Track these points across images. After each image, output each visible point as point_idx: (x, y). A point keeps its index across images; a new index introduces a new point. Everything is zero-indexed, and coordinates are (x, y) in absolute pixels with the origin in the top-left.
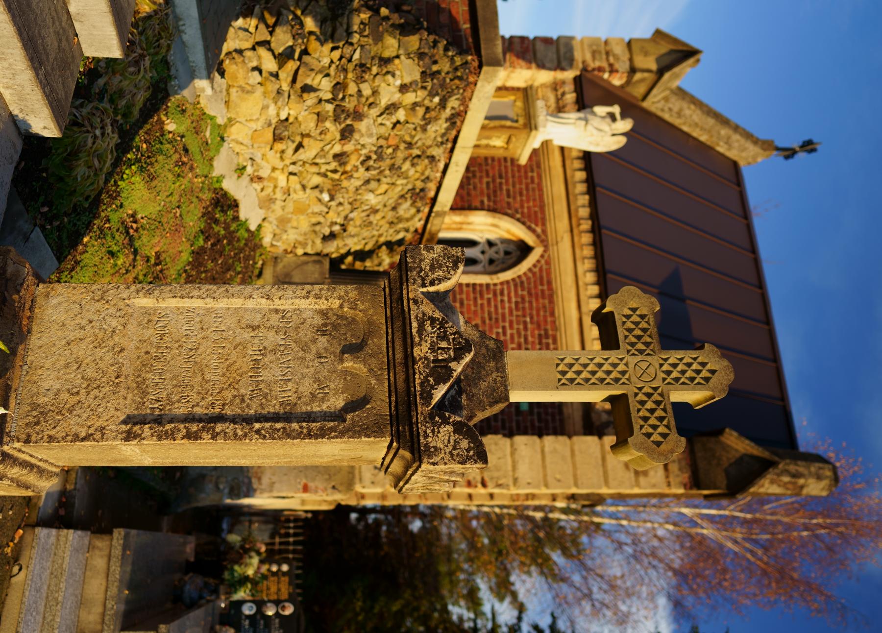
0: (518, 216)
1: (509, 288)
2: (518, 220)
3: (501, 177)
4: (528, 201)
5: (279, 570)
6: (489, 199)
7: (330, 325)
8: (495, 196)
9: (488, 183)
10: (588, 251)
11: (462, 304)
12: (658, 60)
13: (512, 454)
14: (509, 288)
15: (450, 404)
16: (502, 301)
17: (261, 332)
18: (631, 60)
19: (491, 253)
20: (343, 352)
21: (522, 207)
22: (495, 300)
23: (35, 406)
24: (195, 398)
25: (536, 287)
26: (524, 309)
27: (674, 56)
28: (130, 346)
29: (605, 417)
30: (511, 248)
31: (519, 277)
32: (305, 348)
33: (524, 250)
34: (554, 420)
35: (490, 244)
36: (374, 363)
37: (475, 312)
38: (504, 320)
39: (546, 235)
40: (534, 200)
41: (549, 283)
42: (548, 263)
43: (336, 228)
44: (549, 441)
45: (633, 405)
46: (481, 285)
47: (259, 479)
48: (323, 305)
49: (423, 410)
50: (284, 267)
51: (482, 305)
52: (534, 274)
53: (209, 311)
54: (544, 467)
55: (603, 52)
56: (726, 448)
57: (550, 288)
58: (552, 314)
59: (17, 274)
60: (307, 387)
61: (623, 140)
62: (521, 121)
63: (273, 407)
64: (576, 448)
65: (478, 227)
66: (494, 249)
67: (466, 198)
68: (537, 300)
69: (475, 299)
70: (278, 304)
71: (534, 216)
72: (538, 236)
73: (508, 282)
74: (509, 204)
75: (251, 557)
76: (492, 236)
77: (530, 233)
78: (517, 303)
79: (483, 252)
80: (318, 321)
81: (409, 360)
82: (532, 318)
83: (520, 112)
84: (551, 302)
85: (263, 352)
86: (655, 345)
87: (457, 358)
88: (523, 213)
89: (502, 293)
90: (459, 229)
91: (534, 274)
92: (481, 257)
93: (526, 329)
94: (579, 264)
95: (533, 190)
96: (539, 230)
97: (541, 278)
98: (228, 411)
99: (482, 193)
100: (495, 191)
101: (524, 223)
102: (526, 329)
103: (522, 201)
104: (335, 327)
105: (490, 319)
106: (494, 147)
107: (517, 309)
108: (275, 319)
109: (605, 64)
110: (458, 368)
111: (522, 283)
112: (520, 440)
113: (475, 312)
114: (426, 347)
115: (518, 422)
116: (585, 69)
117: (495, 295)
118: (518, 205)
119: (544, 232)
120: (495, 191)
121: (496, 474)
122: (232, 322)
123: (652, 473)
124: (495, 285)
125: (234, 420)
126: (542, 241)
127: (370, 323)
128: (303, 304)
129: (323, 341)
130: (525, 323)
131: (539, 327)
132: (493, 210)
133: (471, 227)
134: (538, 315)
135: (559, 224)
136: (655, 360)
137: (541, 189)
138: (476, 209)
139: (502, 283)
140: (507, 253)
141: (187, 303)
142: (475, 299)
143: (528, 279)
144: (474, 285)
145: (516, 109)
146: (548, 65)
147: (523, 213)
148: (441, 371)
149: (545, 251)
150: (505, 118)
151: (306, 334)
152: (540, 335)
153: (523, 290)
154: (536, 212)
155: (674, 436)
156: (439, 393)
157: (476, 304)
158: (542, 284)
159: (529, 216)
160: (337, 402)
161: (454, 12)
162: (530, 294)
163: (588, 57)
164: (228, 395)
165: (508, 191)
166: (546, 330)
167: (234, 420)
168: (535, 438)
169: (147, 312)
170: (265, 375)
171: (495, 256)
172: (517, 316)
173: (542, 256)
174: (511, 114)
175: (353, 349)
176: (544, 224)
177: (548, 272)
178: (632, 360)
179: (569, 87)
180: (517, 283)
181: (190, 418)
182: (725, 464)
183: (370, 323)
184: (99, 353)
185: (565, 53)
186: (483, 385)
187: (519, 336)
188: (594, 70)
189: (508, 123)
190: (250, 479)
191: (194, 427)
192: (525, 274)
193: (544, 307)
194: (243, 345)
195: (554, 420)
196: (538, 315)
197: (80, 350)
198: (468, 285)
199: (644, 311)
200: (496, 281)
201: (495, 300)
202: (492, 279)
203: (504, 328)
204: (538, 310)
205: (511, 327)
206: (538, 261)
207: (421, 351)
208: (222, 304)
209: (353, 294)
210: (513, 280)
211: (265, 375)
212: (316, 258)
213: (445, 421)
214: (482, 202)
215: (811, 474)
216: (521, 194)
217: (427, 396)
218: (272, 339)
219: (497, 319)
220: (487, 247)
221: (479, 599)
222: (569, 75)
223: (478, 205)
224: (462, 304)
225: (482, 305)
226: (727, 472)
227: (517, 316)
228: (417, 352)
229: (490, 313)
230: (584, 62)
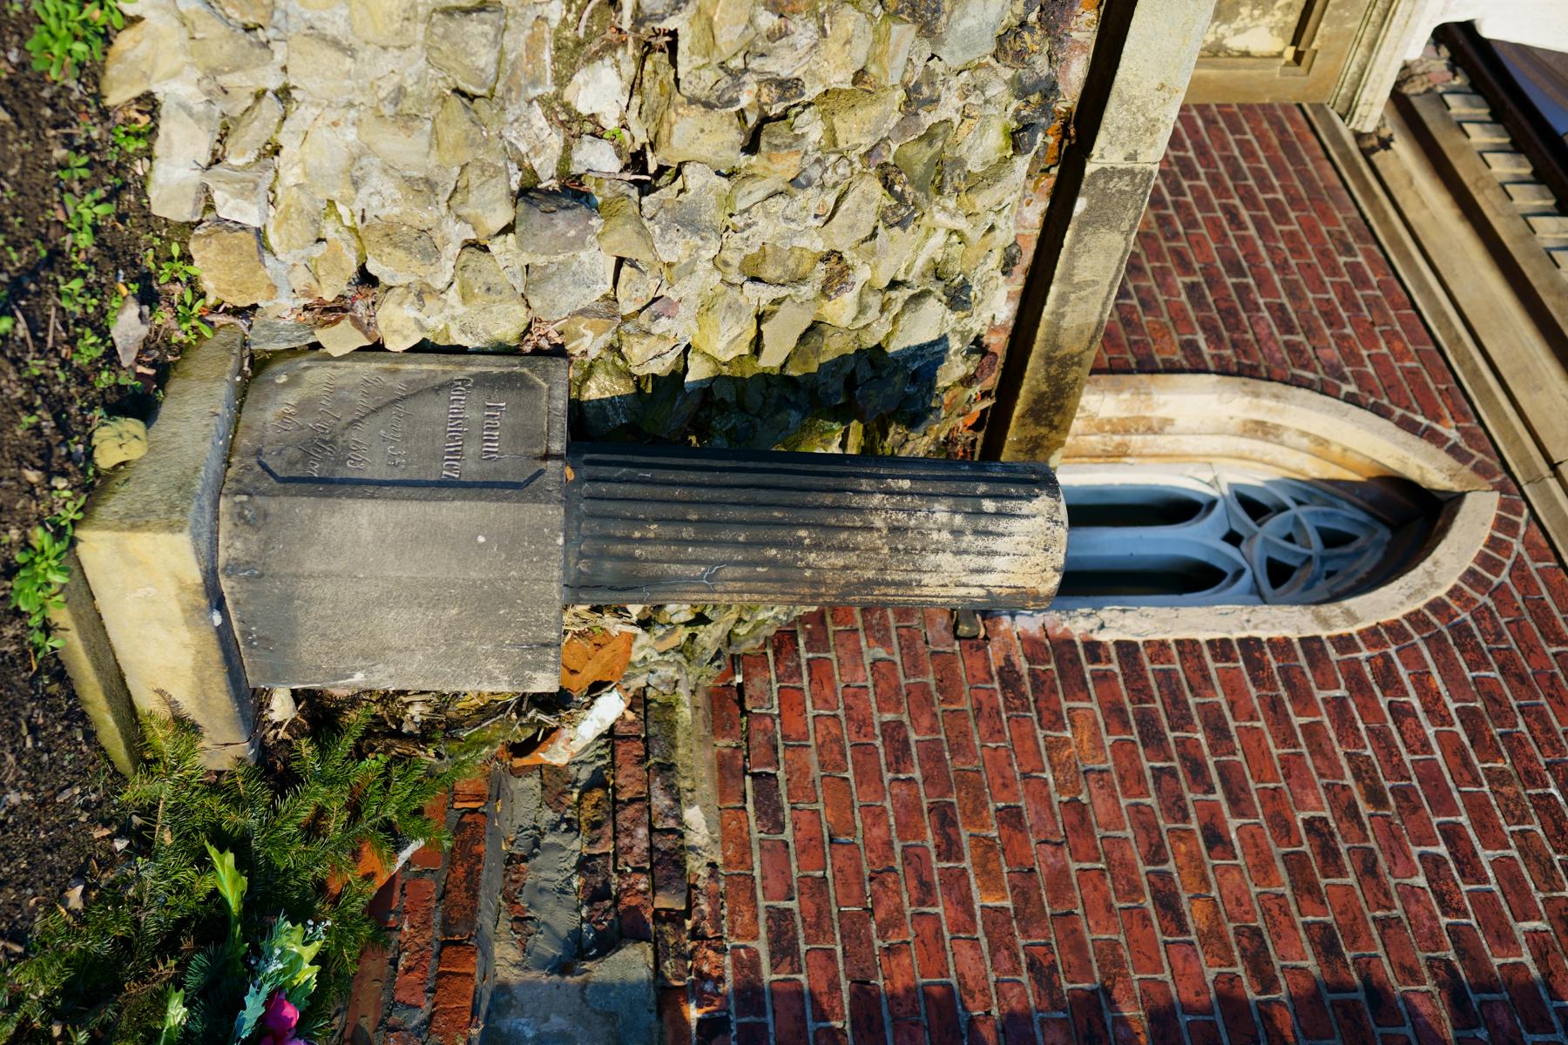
0: (1346, 388)
1: (1411, 656)
2: (1351, 399)
3: (1235, 268)
4: (1370, 341)
6: (1215, 338)
8: (1234, 324)
9: (1192, 289)
11: (1218, 730)
14: (1411, 656)
16: (1401, 713)
30: (1345, 517)
31: (1437, 606)
35: (1254, 507)
37: (1291, 765)
43: (598, 159)
46: (1282, 647)
50: (305, 407)
51: (1311, 731)
65: (1188, 444)
66: (1273, 526)
73: (1395, 630)
76: (1254, 477)
79: (1233, 538)
88: (1361, 378)
89: (1388, 678)
90: (1119, 455)
91: (1500, 593)
99: (1179, 317)
100: (1229, 314)
106: (1246, 54)
113: (1291, 765)
118: (1333, 353)
120: (1229, 314)
124: (1345, 643)
126: (1482, 470)
133: (1162, 442)
138: (1172, 369)
139: (1372, 636)
143: (1481, 614)
144: (1250, 646)
147: (1361, 378)
153: (1478, 663)
157: (1287, 738)
159: (1391, 388)
165: (1278, 311)
171: (1287, 554)
173: (1502, 524)
192: (1455, 592)
198: (1221, 648)
200: (1342, 629)
202: (1325, 622)
205: (1489, 834)
210: (1416, 618)
212: (494, 366)
214: (1190, 347)
216: (1332, 320)
221: (208, 596)
223: (1178, 357)
224: (1218, 730)
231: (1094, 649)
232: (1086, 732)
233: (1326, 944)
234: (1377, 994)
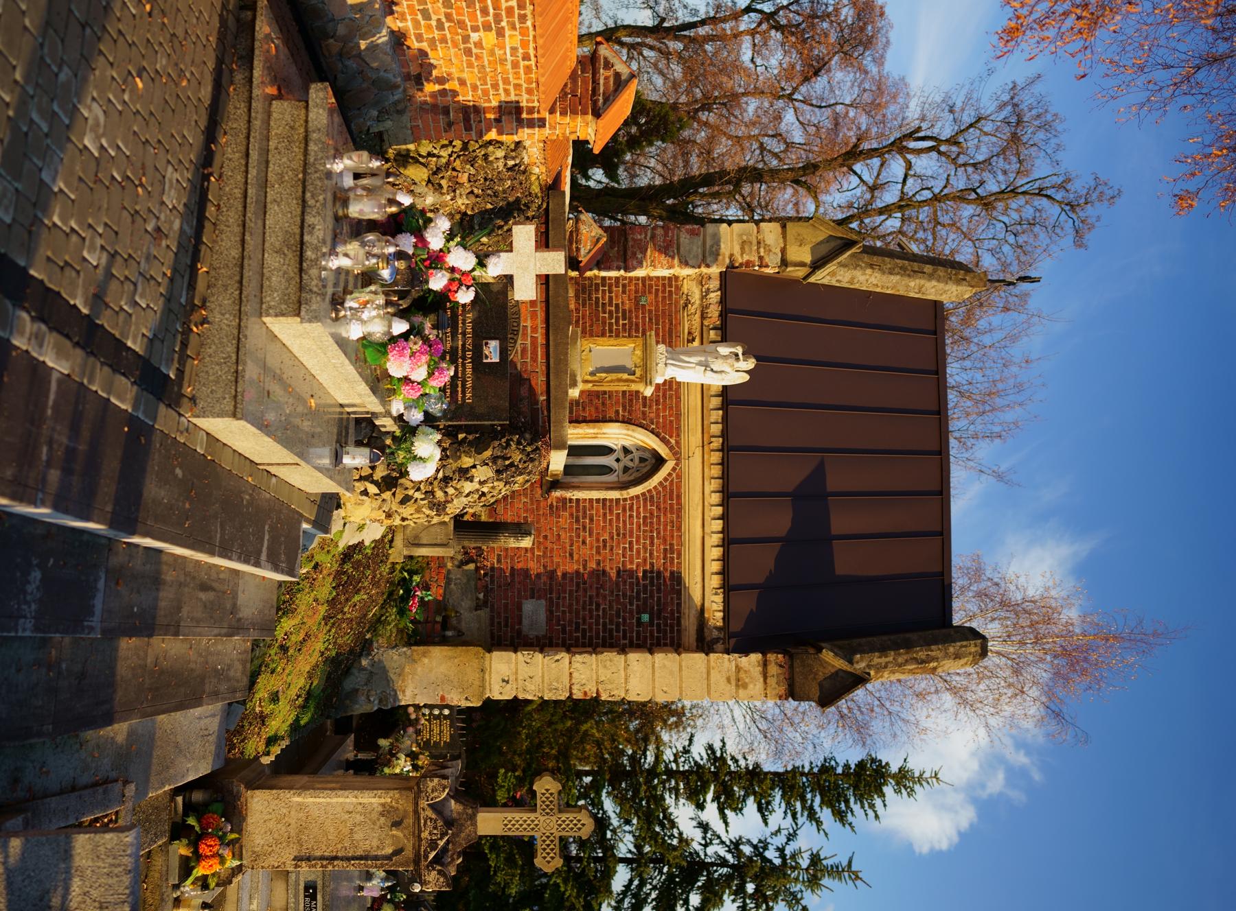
1: (638, 502)
2: (652, 432)
4: (664, 410)
5: (441, 713)
6: (624, 409)
7: (386, 811)
8: (631, 406)
10: (716, 471)
11: (591, 520)
12: (813, 250)
13: (625, 669)
14: (638, 502)
15: (437, 860)
16: (631, 516)
17: (353, 815)
18: (783, 251)
19: (626, 461)
20: (392, 825)
21: (658, 416)
22: (624, 516)
23: (254, 852)
24: (324, 848)
25: (665, 502)
26: (652, 523)
27: (833, 244)
28: (293, 822)
29: (715, 633)
30: (647, 455)
31: (649, 491)
32: (374, 823)
33: (659, 461)
34: (672, 631)
35: (626, 450)
36: (406, 832)
37: (604, 527)
38: (631, 536)
39: (679, 448)
40: (671, 408)
41: (679, 497)
42: (679, 477)
44: (660, 657)
45: (539, 842)
46: (611, 500)
47: (404, 692)
48: (382, 801)
49: (423, 863)
52: (664, 488)
53: (328, 804)
54: (654, 680)
55: (755, 242)
56: (824, 664)
57: (679, 503)
58: (679, 529)
59: (238, 792)
60: (375, 843)
61: (746, 377)
62: (638, 373)
63: (360, 853)
64: (683, 664)
66: (630, 457)
67: (601, 408)
68: (665, 514)
69: (605, 514)
70: (361, 800)
71: (668, 429)
72: (671, 448)
73: (637, 497)
74: (644, 413)
75: (398, 759)
76: (627, 443)
77: (663, 446)
78: (645, 518)
79: (618, 460)
80: (380, 809)
81: (420, 839)
82: (658, 533)
83: (638, 361)
84: (679, 517)
85: (355, 825)
86: (556, 811)
87: (441, 839)
89: (631, 509)
91: (664, 488)
92: (615, 465)
93: (652, 544)
94: (706, 483)
95: (671, 397)
96: (673, 441)
97: (672, 491)
98: (339, 854)
100: (631, 400)
101: (657, 435)
102: (652, 544)
103: (658, 409)
104: (389, 812)
105: (618, 535)
107: (645, 524)
108: (360, 808)
109: (755, 258)
110: (441, 843)
111: (652, 497)
112: (633, 657)
114: (427, 833)
115: (638, 633)
116: (731, 266)
117: (624, 510)
118: (653, 415)
119: (678, 443)
121: (610, 687)
122: (339, 809)
123: (751, 686)
124: (625, 500)
125: (342, 859)
126: (675, 454)
127: (405, 811)
128: (373, 800)
129: (382, 819)
130: (652, 538)
131: (665, 543)
132: (627, 421)
134: (665, 530)
135: (692, 438)
136: (554, 819)
137: (678, 397)
138: (611, 421)
140: (642, 460)
141: (318, 800)
142: (605, 514)
143: (658, 493)
144: (604, 500)
145: (635, 358)
146: (690, 263)
148: (433, 844)
149: (677, 464)
150: (621, 369)
151: (375, 816)
152: (665, 550)
154: (671, 422)
155: (557, 858)
156: (432, 856)
158: (671, 499)
160: (389, 851)
161: (533, 383)
162: (659, 509)
163: (737, 250)
164: (339, 846)
166: (671, 545)
167: (342, 859)
168: (648, 655)
169: (299, 804)
170: (356, 837)
171: (630, 464)
172: (645, 531)
173: (674, 469)
174: (630, 365)
175: (396, 824)
176: (678, 435)
177: (679, 487)
178: (542, 819)
179: (715, 284)
180: (647, 497)
181: (322, 858)
182: (821, 676)
183: (405, 811)
184: (279, 826)
185: (712, 246)
186: (463, 835)
187: (645, 552)
188: (741, 265)
189: (625, 376)
190: (395, 691)
191: (325, 863)
192: (655, 487)
193: (672, 522)
194: (344, 821)
195: (672, 631)
196: (665, 530)
197: (271, 824)
198: (598, 500)
199: (552, 791)
201: (624, 516)
203: (631, 543)
204: (665, 525)
205: (638, 542)
206: (670, 474)
207: (425, 835)
208: (335, 800)
209: (397, 796)
210: (644, 494)
211: (356, 837)
213: (434, 869)
214: (617, 412)
215: (947, 656)
217: (426, 857)
218: (359, 818)
219: (624, 535)
220: (622, 456)
222: (715, 270)
224: (591, 520)
225: (611, 520)
226: (820, 685)
227: (645, 531)
228: (423, 835)
229: (618, 529)
230: (732, 255)
231: (571, 500)
232: (565, 519)
233: (598, 563)
234: (604, 571)
